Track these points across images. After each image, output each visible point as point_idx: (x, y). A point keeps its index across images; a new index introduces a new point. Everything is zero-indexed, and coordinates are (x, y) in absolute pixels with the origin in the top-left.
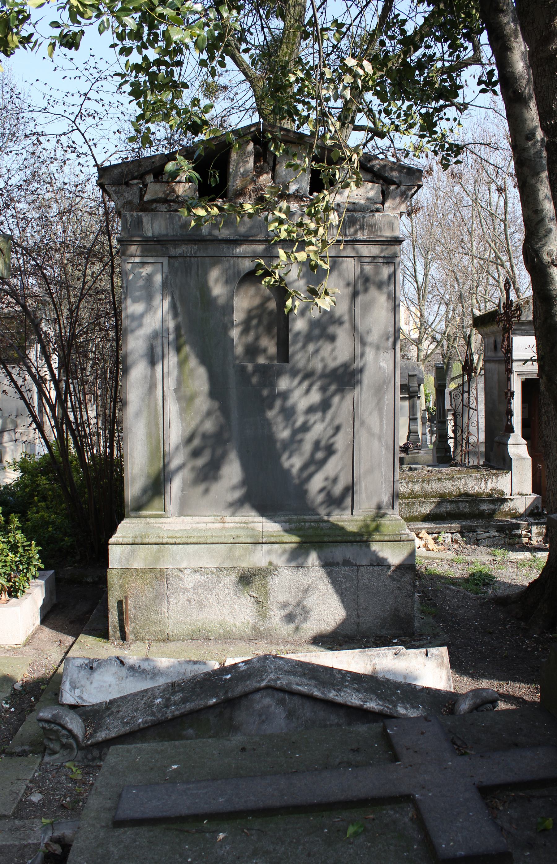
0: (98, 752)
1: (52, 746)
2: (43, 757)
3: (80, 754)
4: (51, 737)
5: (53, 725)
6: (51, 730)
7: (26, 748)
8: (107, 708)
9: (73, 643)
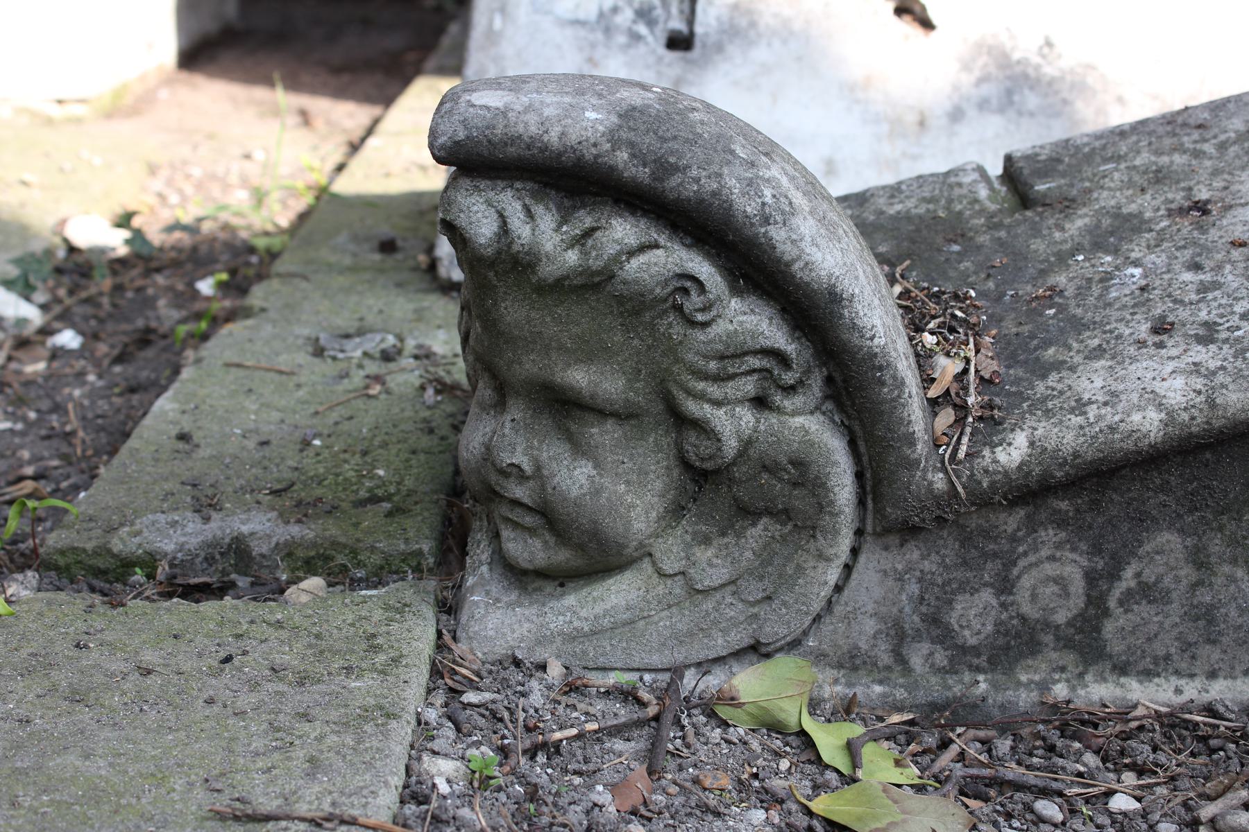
0: (1073, 569)
1: (574, 478)
2: (449, 608)
3: (879, 585)
4: (579, 378)
5: (622, 231)
6: (594, 285)
7: (260, 526)
8: (1224, 105)
9: (370, 131)
